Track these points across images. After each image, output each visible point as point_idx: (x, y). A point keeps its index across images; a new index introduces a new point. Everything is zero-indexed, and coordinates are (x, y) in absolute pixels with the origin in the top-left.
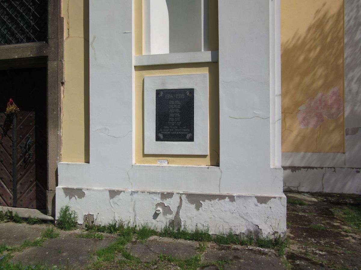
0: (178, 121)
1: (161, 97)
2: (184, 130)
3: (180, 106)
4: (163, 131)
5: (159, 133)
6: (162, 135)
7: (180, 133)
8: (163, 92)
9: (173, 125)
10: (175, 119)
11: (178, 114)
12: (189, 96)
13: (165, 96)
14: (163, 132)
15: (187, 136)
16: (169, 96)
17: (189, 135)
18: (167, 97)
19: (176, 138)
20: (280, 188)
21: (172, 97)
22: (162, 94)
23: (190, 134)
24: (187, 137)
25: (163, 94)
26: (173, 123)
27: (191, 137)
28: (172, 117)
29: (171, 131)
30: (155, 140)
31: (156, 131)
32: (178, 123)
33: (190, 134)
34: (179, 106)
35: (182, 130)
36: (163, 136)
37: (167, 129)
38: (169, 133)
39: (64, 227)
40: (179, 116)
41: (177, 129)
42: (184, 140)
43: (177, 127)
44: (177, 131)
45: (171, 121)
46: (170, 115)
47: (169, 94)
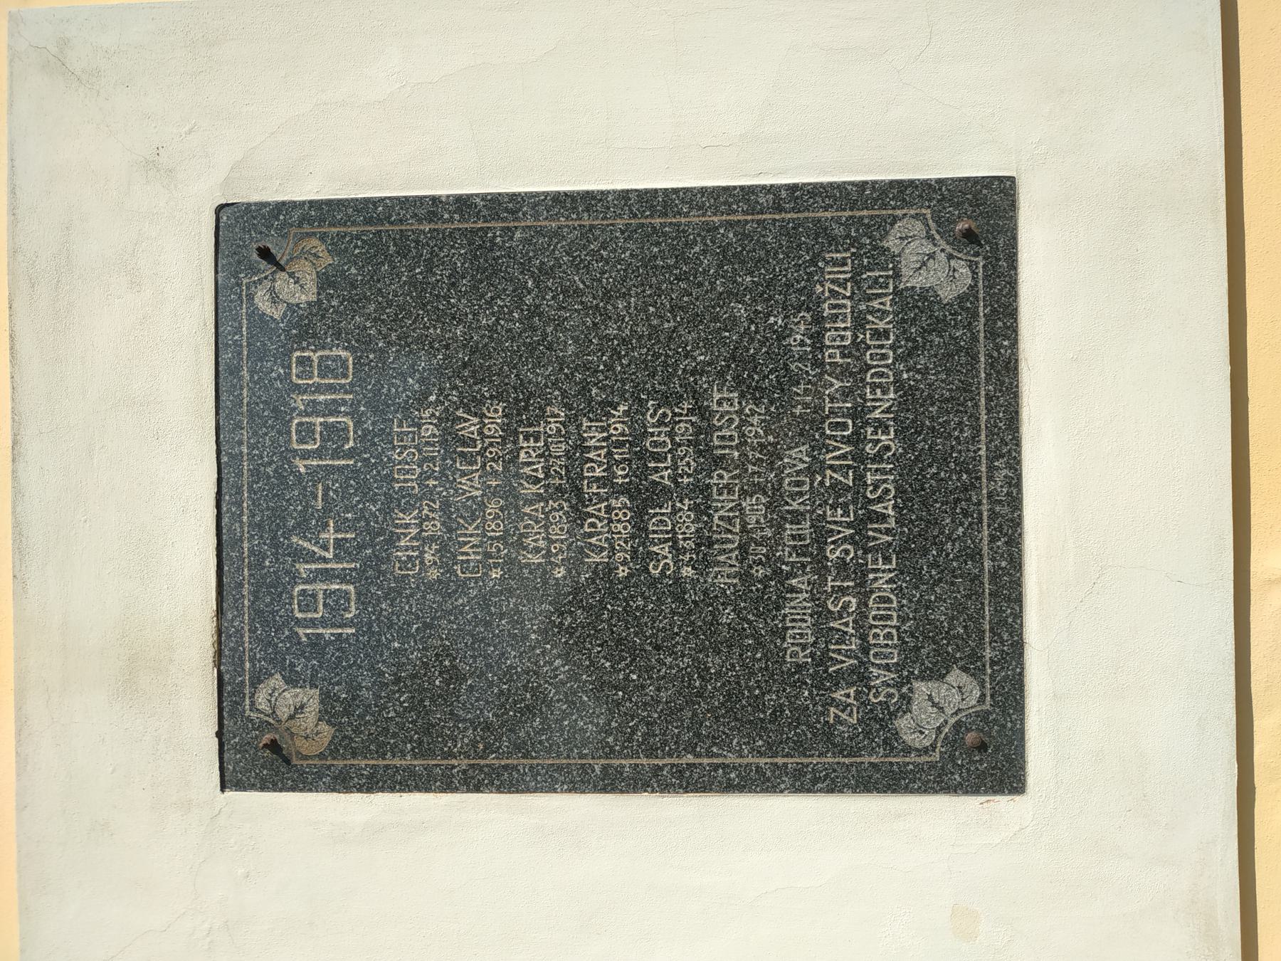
0: (704, 431)
1: (326, 714)
2: (838, 335)
3: (474, 405)
4: (860, 676)
5: (892, 742)
6: (922, 688)
7: (882, 403)
8: (256, 681)
9: (755, 509)
10: (665, 477)
11: (594, 437)
12: (325, 281)
13: (316, 643)
14: (879, 677)
15: (926, 297)
16: (327, 575)
17: (912, 254)
18: (336, 603)
19: (968, 467)
20: (265, 253)
21: (330, 535)
22: (290, 698)
23: (892, 243)
24: (948, 293)
25: (292, 681)
26: (723, 504)
27: (944, 224)
28: (640, 529)
29: (859, 540)
30: (1003, 803)
31: (867, 783)
32: (724, 434)
33: (892, 243)
34: (470, 427)
35: (844, 372)
36: (936, 674)
37: (821, 614)
38: (882, 582)
39: (751, 562)
40: (618, 428)
41: (818, 447)
42: (992, 334)
43: (799, 455)
44: (857, 439)
45: (704, 542)
46: (610, 569)
47: (294, 578)
